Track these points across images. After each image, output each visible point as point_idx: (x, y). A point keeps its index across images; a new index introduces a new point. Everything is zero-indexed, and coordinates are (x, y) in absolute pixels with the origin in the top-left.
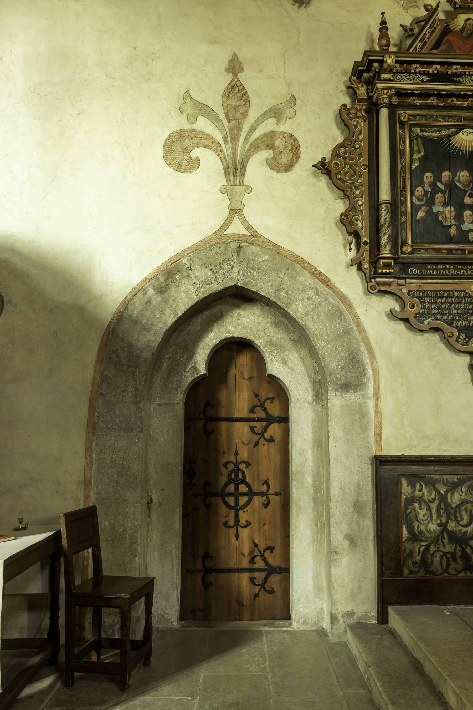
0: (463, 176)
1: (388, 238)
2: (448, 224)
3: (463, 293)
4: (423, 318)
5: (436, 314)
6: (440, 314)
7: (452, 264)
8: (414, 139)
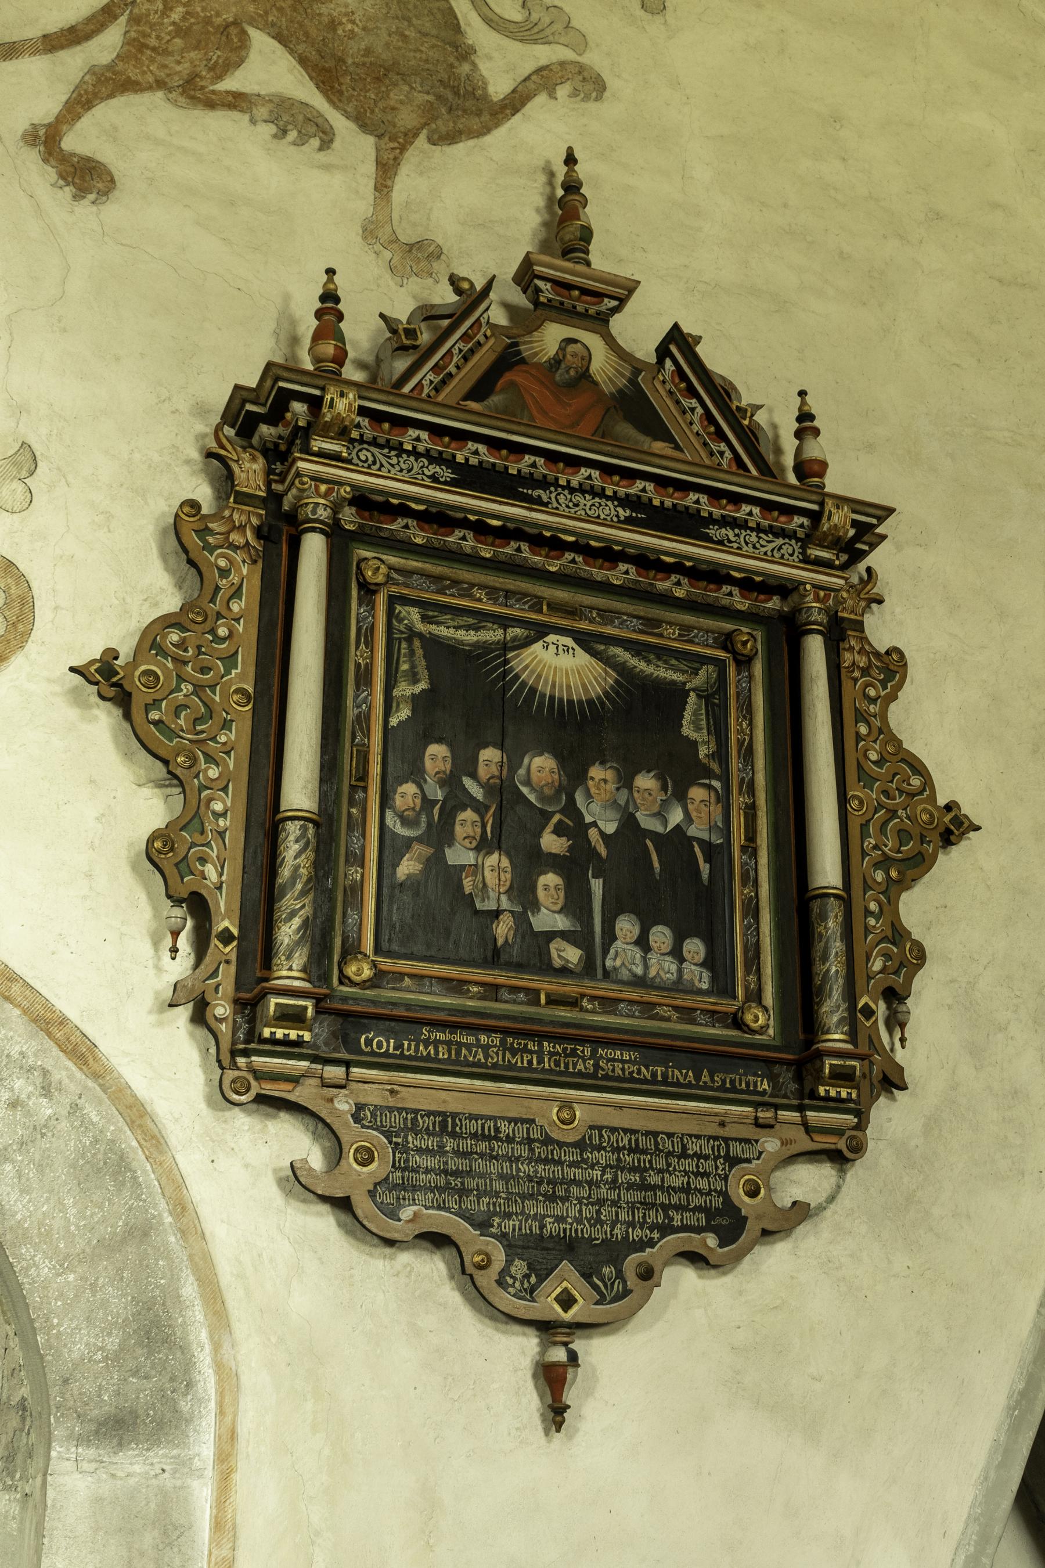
0: (540, 770)
1: (299, 930)
2: (491, 905)
5: (441, 1190)
6: (452, 1189)
8: (400, 639)
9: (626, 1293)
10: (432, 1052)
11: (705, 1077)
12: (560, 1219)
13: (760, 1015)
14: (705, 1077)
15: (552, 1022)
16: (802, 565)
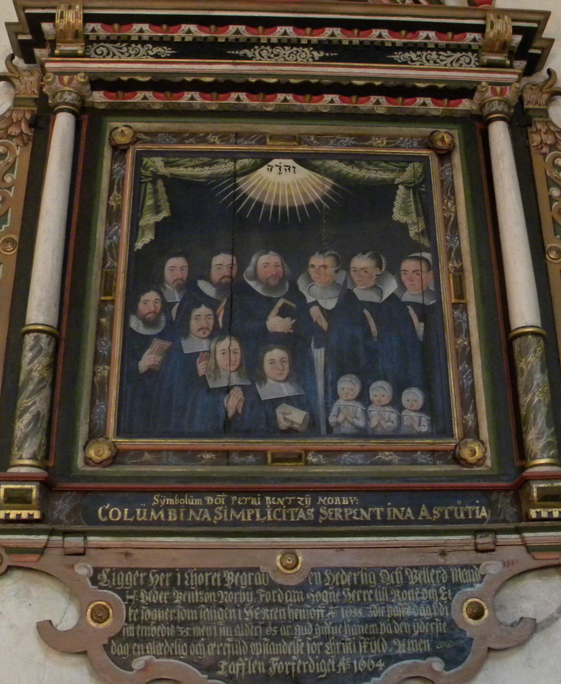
0: (267, 265)
1: (29, 424)
2: (222, 383)
3: (250, 574)
4: (131, 650)
5: (171, 639)
6: (181, 637)
7: (220, 492)
8: (146, 183)
10: (162, 516)
11: (424, 512)
12: (286, 657)
13: (477, 448)
14: (424, 512)
15: (273, 478)
16: (478, 69)
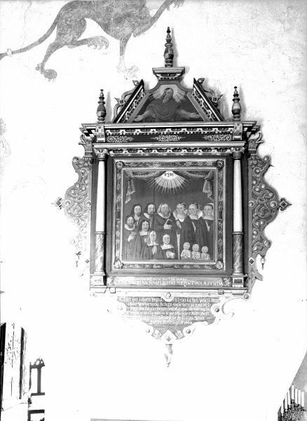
9: (183, 337)
